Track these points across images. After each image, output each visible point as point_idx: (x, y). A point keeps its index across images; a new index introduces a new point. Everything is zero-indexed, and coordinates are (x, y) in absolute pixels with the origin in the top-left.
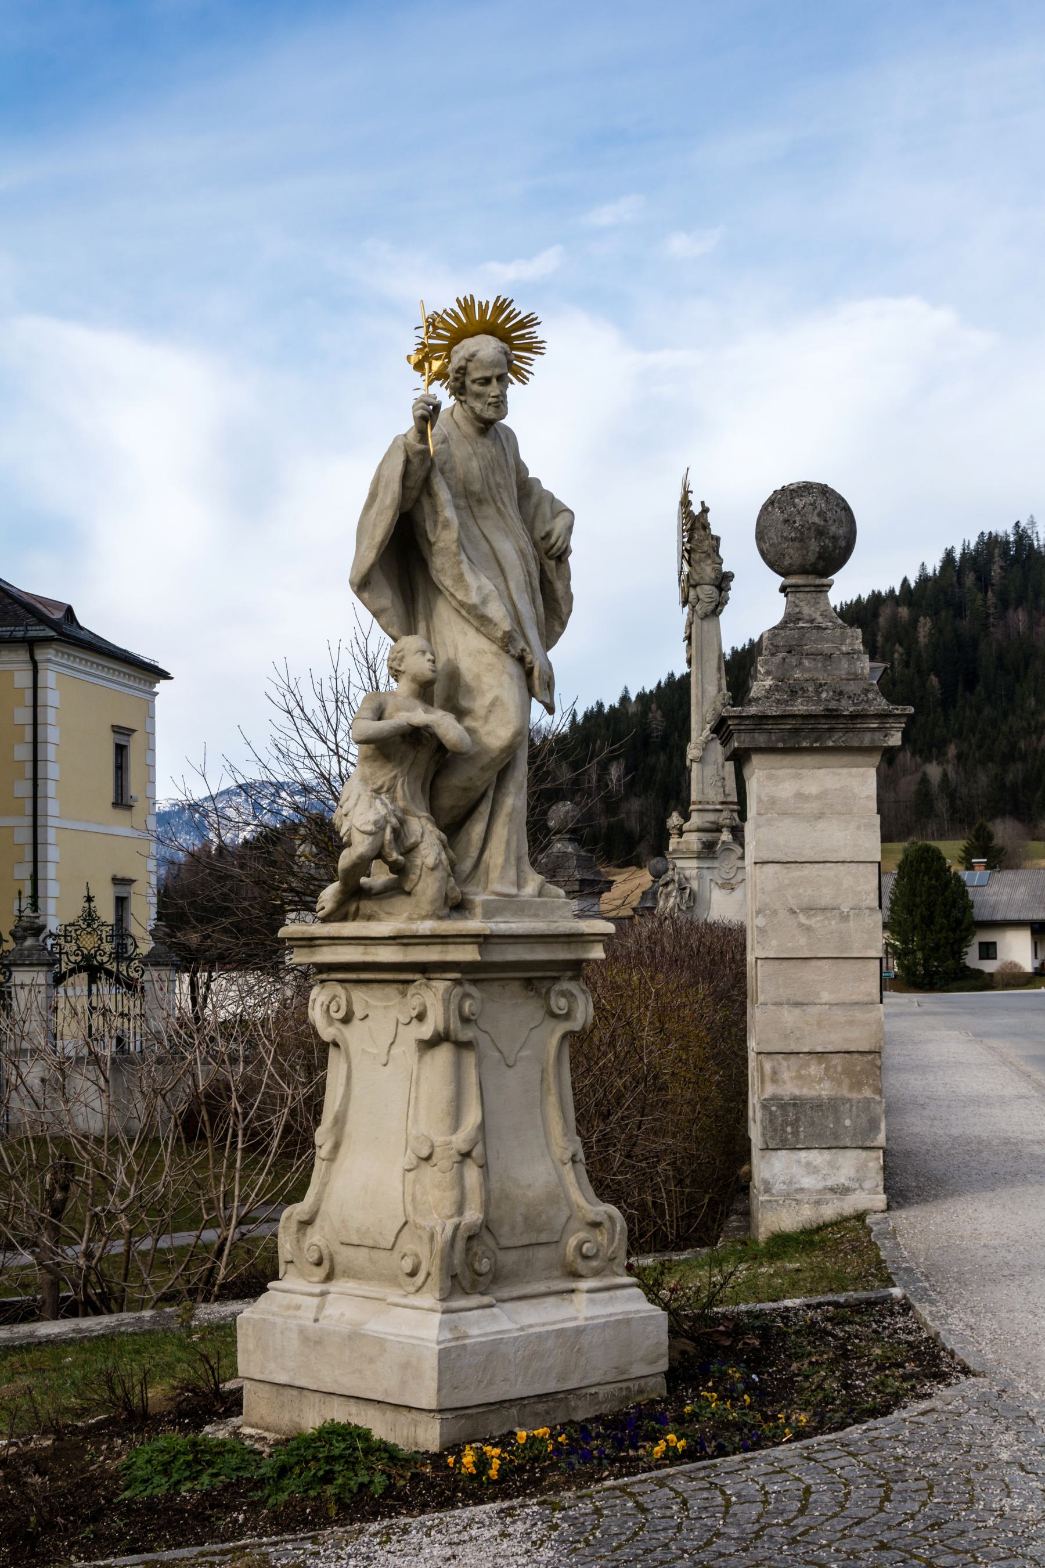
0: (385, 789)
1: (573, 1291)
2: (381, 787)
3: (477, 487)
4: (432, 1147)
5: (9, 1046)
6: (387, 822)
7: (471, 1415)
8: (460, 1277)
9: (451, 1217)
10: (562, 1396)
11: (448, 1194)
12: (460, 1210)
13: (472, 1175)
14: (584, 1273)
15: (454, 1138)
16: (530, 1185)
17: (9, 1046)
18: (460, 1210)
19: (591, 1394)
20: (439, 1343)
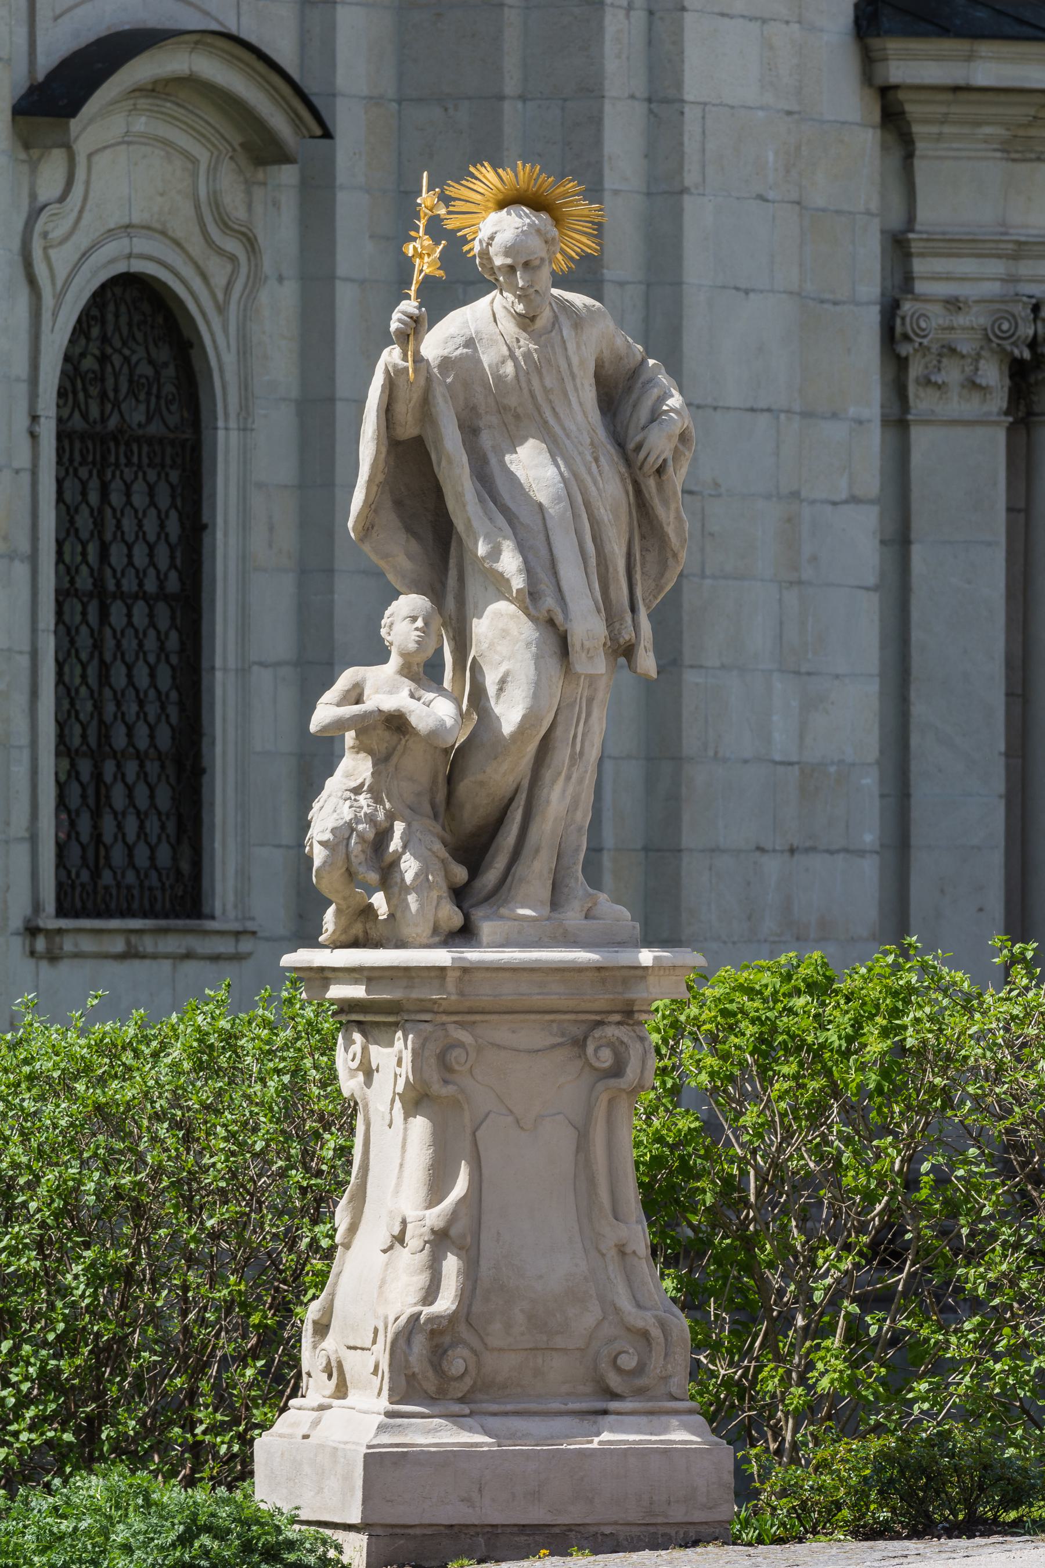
0: (365, 788)
1: (605, 1412)
2: (362, 785)
3: (512, 401)
4: (404, 1223)
5: (1041, 1026)
6: (353, 830)
7: (415, 1537)
8: (420, 1377)
9: (415, 1304)
10: (557, 1530)
11: (415, 1279)
12: (430, 1294)
13: (451, 1264)
14: (619, 1390)
15: (428, 1212)
16: (541, 1277)
17: (1041, 1026)
18: (430, 1294)
19: (603, 1534)
20: (369, 1447)
